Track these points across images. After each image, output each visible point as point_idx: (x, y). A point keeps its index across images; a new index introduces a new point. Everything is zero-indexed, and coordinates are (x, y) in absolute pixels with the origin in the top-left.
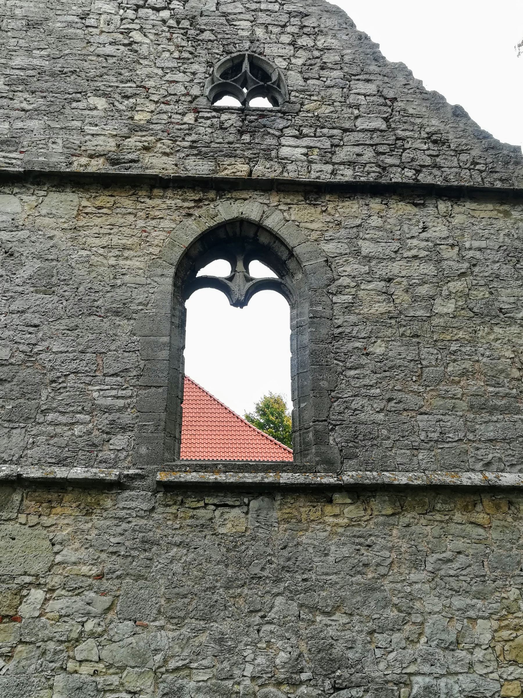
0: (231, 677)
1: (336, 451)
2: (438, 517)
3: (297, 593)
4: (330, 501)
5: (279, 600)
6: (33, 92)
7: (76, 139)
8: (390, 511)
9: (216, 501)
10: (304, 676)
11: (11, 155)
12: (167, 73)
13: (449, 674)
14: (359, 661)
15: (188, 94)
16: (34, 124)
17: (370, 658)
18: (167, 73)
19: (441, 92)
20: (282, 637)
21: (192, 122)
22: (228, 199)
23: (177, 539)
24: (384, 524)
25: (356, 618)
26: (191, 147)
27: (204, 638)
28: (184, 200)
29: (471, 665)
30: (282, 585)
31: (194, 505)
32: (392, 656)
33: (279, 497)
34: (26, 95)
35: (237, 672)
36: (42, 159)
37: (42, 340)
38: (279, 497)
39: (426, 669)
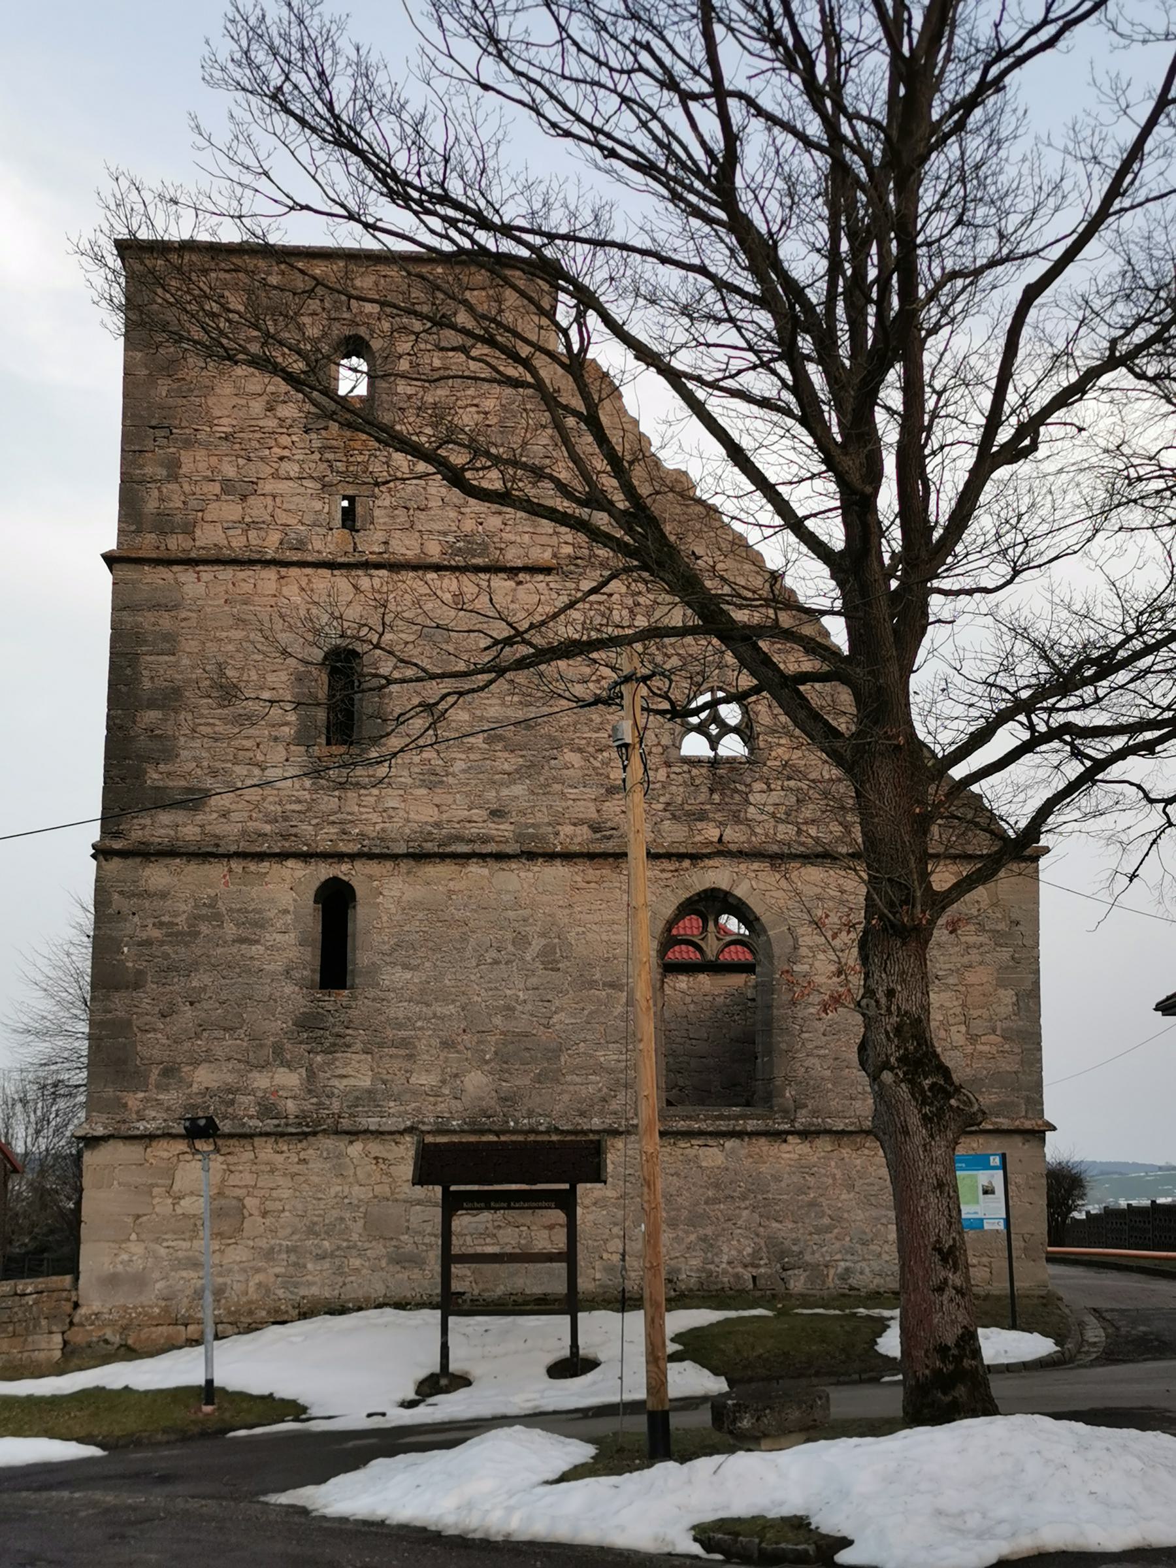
0: (712, 1263)
1: (791, 1102)
2: (866, 1152)
3: (758, 1207)
4: (785, 1141)
5: (745, 1213)
6: (512, 751)
7: (559, 805)
8: (829, 1149)
9: (699, 1143)
10: (762, 1262)
11: (502, 827)
12: (810, 948)
13: (864, 1260)
14: (801, 1252)
15: (659, 744)
16: (518, 790)
17: (809, 1250)
18: (810, 948)
19: (1023, 287)
20: (746, 1237)
21: (664, 779)
22: (702, 868)
23: (672, 1171)
24: (824, 1158)
25: (800, 1224)
26: (665, 810)
27: (693, 1237)
28: (663, 871)
29: (880, 1254)
30: (747, 1203)
31: (683, 1145)
32: (824, 1249)
33: (746, 1139)
34: (506, 755)
35: (716, 1260)
36: (531, 830)
37: (555, 1013)
38: (746, 1139)
39: (849, 1257)
